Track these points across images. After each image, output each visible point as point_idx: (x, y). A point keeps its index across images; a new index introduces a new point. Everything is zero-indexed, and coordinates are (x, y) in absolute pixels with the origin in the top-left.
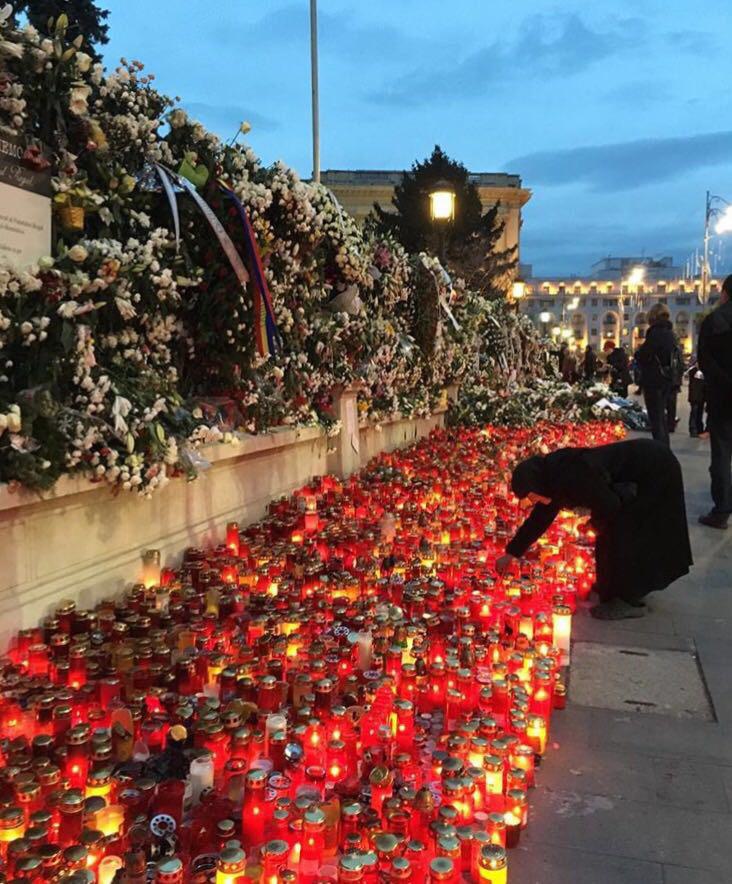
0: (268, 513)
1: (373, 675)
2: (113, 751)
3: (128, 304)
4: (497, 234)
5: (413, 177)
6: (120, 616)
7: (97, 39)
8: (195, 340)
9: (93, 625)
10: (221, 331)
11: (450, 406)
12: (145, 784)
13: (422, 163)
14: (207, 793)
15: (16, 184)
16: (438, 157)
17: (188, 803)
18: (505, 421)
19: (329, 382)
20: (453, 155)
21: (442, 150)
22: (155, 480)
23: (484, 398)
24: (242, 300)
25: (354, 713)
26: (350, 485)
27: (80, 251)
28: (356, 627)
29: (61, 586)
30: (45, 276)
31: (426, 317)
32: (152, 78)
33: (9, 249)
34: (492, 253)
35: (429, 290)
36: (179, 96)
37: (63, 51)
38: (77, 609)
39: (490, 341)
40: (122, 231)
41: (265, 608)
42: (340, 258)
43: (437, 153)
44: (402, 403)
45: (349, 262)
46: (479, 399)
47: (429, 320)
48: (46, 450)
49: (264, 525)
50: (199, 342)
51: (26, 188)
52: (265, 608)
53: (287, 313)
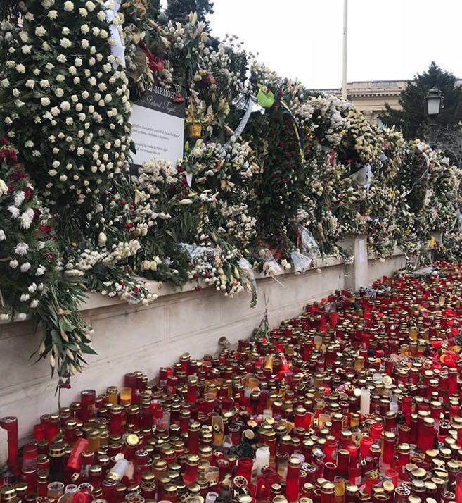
0: (304, 311)
2: (213, 438)
5: (414, 84)
6: (215, 365)
7: (207, 11)
12: (231, 457)
13: (421, 74)
14: (265, 469)
15: (166, 111)
16: (434, 71)
17: (255, 473)
21: (437, 64)
24: (291, 177)
25: (357, 437)
26: (387, 188)
31: (419, 184)
33: (161, 149)
36: (259, 52)
38: (191, 359)
47: (420, 186)
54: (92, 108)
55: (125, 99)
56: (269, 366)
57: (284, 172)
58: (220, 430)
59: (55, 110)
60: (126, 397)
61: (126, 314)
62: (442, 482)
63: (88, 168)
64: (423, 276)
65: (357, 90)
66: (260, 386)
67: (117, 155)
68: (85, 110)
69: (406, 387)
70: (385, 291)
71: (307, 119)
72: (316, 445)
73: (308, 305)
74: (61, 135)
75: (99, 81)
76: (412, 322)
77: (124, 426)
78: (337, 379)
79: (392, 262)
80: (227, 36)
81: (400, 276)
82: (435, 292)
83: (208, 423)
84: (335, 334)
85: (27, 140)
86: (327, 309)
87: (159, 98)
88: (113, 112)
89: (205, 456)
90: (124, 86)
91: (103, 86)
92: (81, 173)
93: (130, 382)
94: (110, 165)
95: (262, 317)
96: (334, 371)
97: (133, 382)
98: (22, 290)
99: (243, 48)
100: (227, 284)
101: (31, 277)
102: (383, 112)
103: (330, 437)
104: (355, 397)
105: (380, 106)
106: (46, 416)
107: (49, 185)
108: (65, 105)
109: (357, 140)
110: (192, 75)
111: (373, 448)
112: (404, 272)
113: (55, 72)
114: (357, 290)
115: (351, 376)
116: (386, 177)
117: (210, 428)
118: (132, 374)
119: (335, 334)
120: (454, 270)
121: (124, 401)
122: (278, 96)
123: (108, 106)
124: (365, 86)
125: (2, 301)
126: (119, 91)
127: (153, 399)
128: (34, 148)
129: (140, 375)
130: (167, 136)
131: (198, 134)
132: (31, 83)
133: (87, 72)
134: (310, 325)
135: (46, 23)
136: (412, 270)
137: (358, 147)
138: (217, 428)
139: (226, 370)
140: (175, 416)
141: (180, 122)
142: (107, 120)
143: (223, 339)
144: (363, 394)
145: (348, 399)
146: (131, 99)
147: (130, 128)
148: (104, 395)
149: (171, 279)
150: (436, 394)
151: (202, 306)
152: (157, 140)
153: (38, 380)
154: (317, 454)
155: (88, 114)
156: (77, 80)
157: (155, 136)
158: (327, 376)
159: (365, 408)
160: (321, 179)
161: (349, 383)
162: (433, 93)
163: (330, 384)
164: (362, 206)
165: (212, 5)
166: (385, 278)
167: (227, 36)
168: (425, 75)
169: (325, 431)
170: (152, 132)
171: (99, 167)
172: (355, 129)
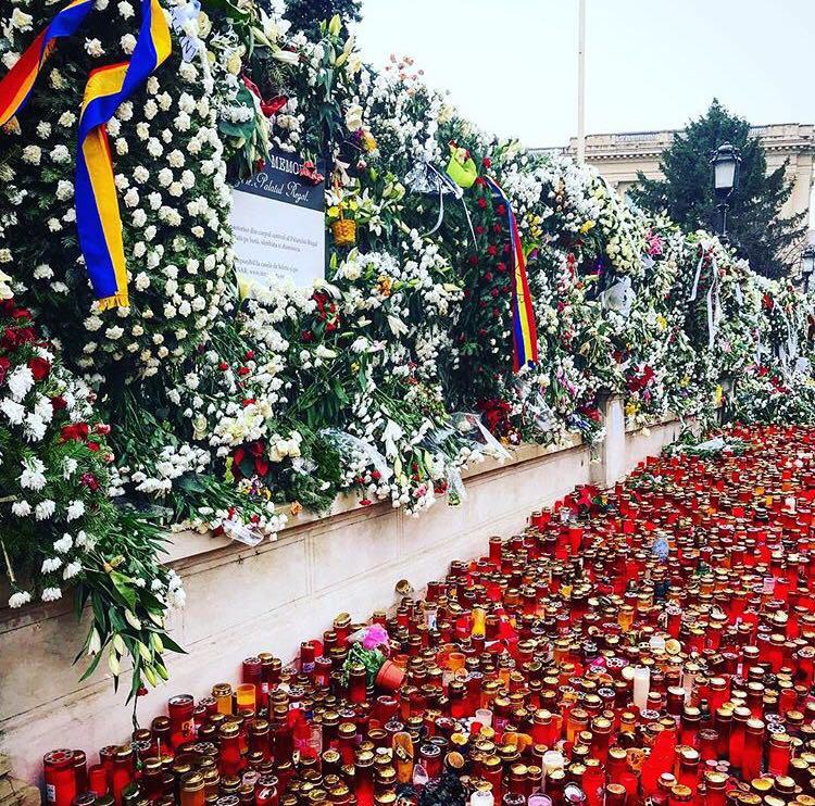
1: (650, 714)
3: (399, 321)
4: (783, 198)
5: (684, 136)
8: (461, 351)
11: (724, 403)
13: (696, 121)
15: (291, 201)
16: (716, 113)
18: (789, 420)
19: (595, 386)
20: (735, 109)
21: (720, 103)
22: (421, 500)
23: (762, 394)
27: (352, 267)
28: (634, 660)
30: (321, 297)
32: (421, 73)
34: (776, 220)
37: (337, 57)
40: (391, 242)
41: (533, 630)
42: (611, 249)
43: (715, 105)
44: (672, 403)
45: (620, 253)
48: (101, 365)
49: (526, 538)
51: (301, 204)
52: (533, 630)
53: (553, 312)
54: (155, 199)
55: (220, 180)
56: (479, 629)
57: (496, 298)
58: (408, 757)
60: (248, 699)
61: (241, 560)
63: (159, 311)
64: (709, 454)
66: (468, 666)
67: (210, 285)
68: (144, 204)
69: (704, 656)
70: (654, 482)
72: (570, 778)
73: (534, 514)
75: (168, 148)
76: (702, 537)
77: (245, 755)
78: (590, 647)
79: (661, 432)
80: (393, 59)
81: (674, 455)
82: (731, 481)
83: (386, 743)
84: (581, 563)
85: (39, 264)
86: (565, 517)
87: (280, 178)
88: (197, 206)
90: (217, 156)
91: (177, 158)
92: (148, 323)
93: (253, 673)
94: (200, 303)
96: (584, 632)
97: (259, 673)
99: (421, 79)
101: (59, 525)
102: (634, 184)
103: (592, 762)
104: (624, 680)
105: (629, 172)
106: (111, 749)
107: (90, 347)
110: (322, 136)
111: (663, 780)
114: (611, 484)
115: (614, 640)
117: (390, 751)
118: (254, 660)
119: (581, 563)
120: (755, 442)
121: (243, 707)
122: (483, 165)
123: (188, 195)
124: (607, 140)
125: (10, 570)
126: (207, 167)
127: (293, 700)
128: (54, 280)
129: (268, 661)
130: (295, 244)
131: (351, 237)
132: (33, 153)
133: (143, 130)
134: (540, 547)
138: (402, 753)
139: (410, 640)
140: (331, 735)
141: (314, 222)
142: (189, 222)
143: (402, 584)
144: (639, 676)
145: (613, 684)
146: (231, 179)
147: (230, 233)
148: (209, 701)
151: (368, 533)
152: (277, 253)
153: (90, 690)
154: (573, 796)
155: (149, 211)
157: (274, 245)
158: (574, 642)
159: (642, 694)
160: (553, 305)
161: (612, 654)
162: (724, 152)
163: (580, 657)
164: (620, 347)
165: (358, 6)
166: (650, 459)
167: (393, 59)
168: (703, 121)
169: (582, 750)
170: (269, 240)
171: (178, 307)
172: (607, 218)
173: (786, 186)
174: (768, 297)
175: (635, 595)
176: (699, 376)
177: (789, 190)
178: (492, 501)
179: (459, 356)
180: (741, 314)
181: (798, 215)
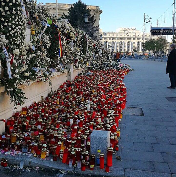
5: (73, 7)
8: (50, 54)
9: (39, 105)
10: (54, 52)
13: (76, 3)
16: (80, 2)
29: (30, 99)
35: (86, 40)
39: (96, 51)
45: (72, 36)
46: (94, 64)
50: (50, 54)
59: (13, 32)
62: (112, 120)
65: (51, 6)
71: (60, 28)
74: (14, 39)
80: (40, 3)
89: (22, 138)
95: (51, 89)
98: (14, 82)
100: (45, 80)
102: (62, 15)
108: (15, 30)
109: (70, 33)
112: (82, 74)
113: (12, 21)
114: (72, 80)
116: (76, 45)
122: (53, 20)
132: (6, 24)
135: (9, 6)
136: (84, 73)
137: (71, 35)
149: (32, 79)
150: (105, 104)
156: (17, 23)
167: (40, 3)
173: (94, 19)
174: (95, 44)
175: (62, 119)
176: (84, 60)
177: (95, 20)
178: (58, 80)
179: (49, 55)
180: (90, 48)
181: (97, 26)
